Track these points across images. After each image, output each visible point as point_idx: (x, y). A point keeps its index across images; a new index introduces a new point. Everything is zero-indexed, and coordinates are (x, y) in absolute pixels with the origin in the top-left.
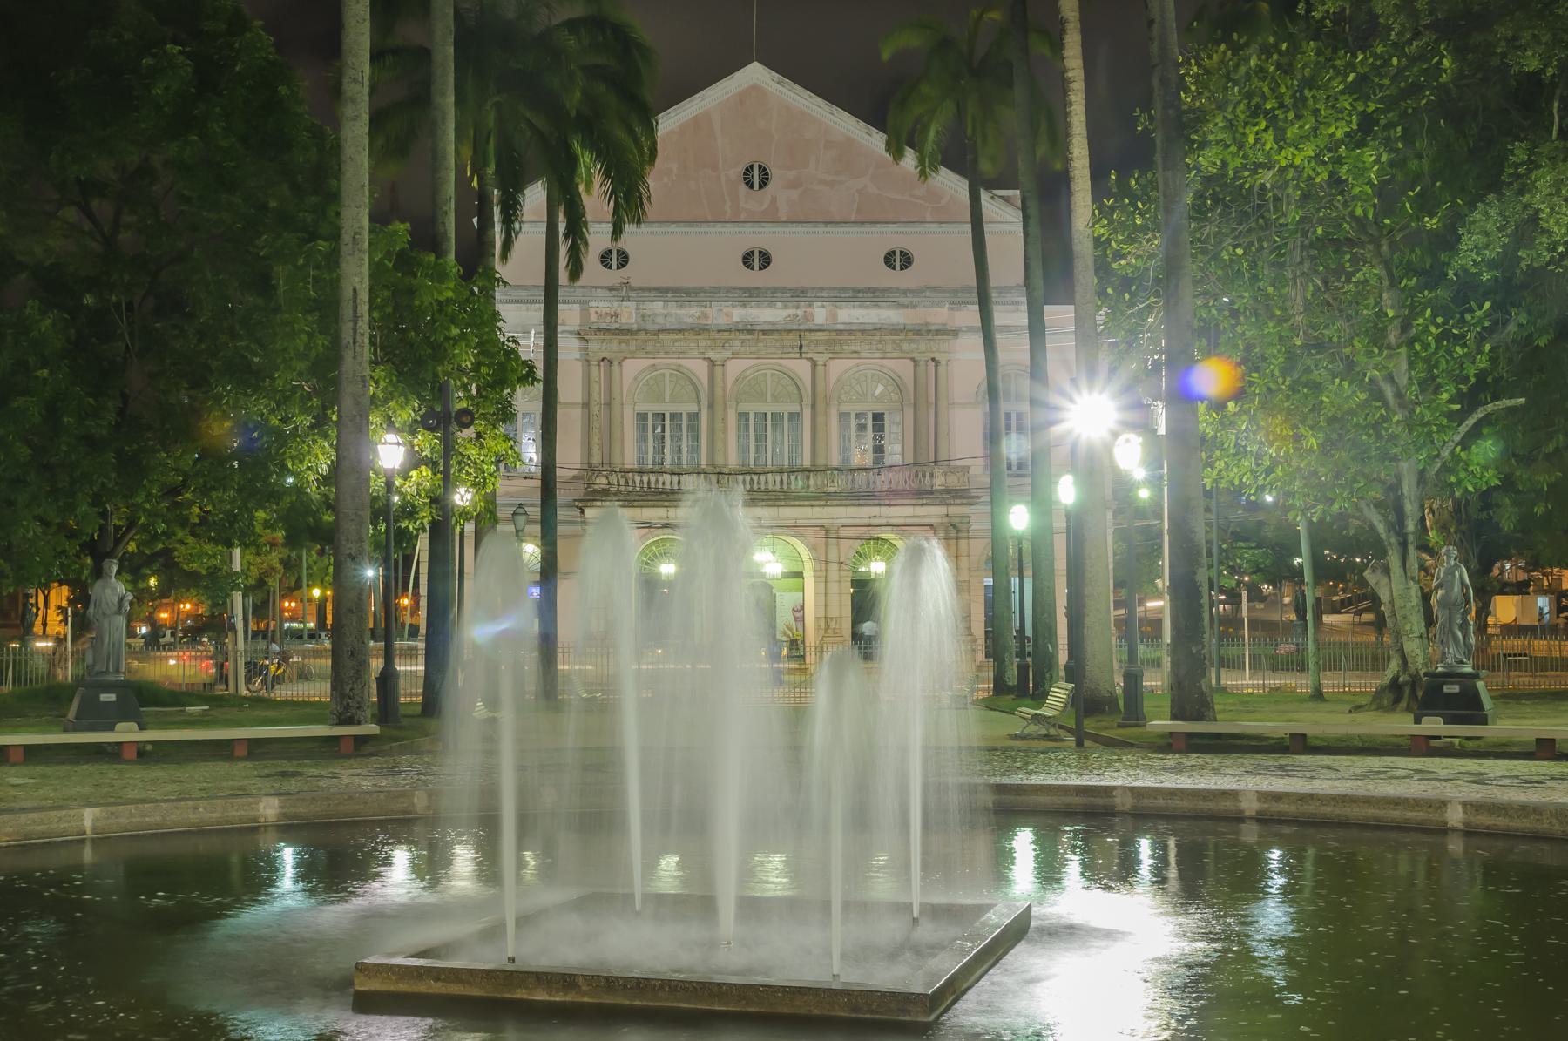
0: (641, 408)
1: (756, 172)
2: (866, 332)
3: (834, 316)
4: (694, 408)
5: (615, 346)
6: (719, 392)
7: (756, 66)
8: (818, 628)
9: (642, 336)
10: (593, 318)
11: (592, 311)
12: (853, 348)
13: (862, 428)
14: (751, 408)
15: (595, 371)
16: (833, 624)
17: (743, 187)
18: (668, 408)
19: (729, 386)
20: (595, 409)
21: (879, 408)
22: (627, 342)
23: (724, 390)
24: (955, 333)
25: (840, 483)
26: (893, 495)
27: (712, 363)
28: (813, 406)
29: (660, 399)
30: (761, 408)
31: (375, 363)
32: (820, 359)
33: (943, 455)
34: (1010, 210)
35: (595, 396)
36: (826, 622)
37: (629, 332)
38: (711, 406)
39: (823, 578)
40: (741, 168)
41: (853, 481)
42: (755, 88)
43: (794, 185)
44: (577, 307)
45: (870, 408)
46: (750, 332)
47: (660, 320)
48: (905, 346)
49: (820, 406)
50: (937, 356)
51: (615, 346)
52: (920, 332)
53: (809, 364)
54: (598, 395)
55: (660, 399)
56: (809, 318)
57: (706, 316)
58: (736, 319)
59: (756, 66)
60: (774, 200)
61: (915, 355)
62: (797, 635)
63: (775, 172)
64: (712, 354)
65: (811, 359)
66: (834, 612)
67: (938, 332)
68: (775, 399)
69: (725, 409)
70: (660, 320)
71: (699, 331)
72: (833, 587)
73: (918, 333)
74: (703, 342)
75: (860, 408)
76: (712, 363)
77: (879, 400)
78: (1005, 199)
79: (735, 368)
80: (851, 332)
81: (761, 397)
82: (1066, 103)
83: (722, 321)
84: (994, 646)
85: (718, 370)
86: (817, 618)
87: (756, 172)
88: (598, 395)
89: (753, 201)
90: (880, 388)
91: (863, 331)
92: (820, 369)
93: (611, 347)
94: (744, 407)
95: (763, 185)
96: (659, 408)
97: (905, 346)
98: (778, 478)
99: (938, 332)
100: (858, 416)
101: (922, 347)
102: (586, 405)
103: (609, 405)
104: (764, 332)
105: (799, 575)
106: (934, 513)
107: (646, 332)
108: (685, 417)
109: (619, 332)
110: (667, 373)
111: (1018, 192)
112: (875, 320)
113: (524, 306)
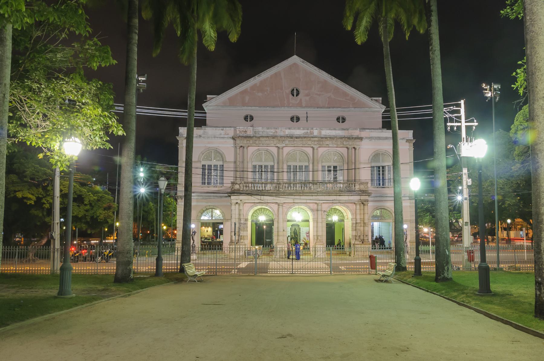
0: (254, 163)
1: (295, 91)
2: (332, 138)
3: (320, 133)
4: (272, 164)
5: (245, 142)
6: (281, 158)
7: (295, 56)
8: (314, 239)
9: (254, 139)
10: (238, 132)
11: (238, 130)
12: (327, 143)
13: (329, 171)
14: (292, 164)
15: (238, 150)
16: (319, 238)
17: (291, 96)
18: (263, 164)
19: (284, 156)
20: (238, 163)
21: (335, 164)
22: (249, 141)
23: (283, 157)
24: (361, 139)
25: (321, 188)
26: (340, 192)
27: (278, 148)
28: (313, 163)
29: (261, 161)
30: (295, 164)
31: (88, 84)
32: (316, 147)
33: (357, 178)
34: (377, 104)
35: (238, 159)
36: (317, 237)
37: (250, 137)
38: (278, 163)
39: (316, 221)
40: (290, 90)
41: (327, 187)
42: (295, 64)
43: (307, 95)
44: (232, 129)
45: (333, 164)
46: (292, 137)
47: (261, 133)
48: (345, 143)
49: (315, 163)
50: (355, 147)
51: (245, 142)
52: (350, 138)
53: (311, 149)
54: (239, 159)
55: (261, 161)
56: (312, 133)
57: (276, 132)
58: (287, 133)
59: (295, 56)
60: (301, 100)
61: (348, 146)
62: (307, 241)
63: (301, 91)
64: (278, 145)
65: (312, 147)
66: (320, 233)
67: (356, 138)
68: (300, 161)
69: (283, 163)
70: (261, 133)
71: (274, 137)
72: (320, 225)
73: (349, 138)
74: (276, 141)
75: (329, 164)
76: (278, 148)
77: (335, 161)
78: (376, 100)
79: (286, 150)
80: (326, 138)
81: (295, 160)
82: (388, 83)
83: (282, 134)
84: (169, 282)
85: (281, 150)
86: (314, 236)
87: (295, 91)
88: (239, 159)
89: (294, 100)
90: (336, 158)
91: (330, 138)
92: (315, 150)
93: (244, 142)
94: (289, 164)
95: (297, 95)
96: (260, 164)
97: (345, 143)
98: (300, 185)
99: (356, 138)
100: (328, 167)
101: (350, 143)
102: (235, 162)
103: (243, 162)
104: (296, 138)
105: (308, 221)
106: (356, 198)
107: (256, 137)
108: (269, 167)
109: (246, 137)
110: (263, 151)
111: (381, 98)
112: (334, 134)
113: (214, 129)
